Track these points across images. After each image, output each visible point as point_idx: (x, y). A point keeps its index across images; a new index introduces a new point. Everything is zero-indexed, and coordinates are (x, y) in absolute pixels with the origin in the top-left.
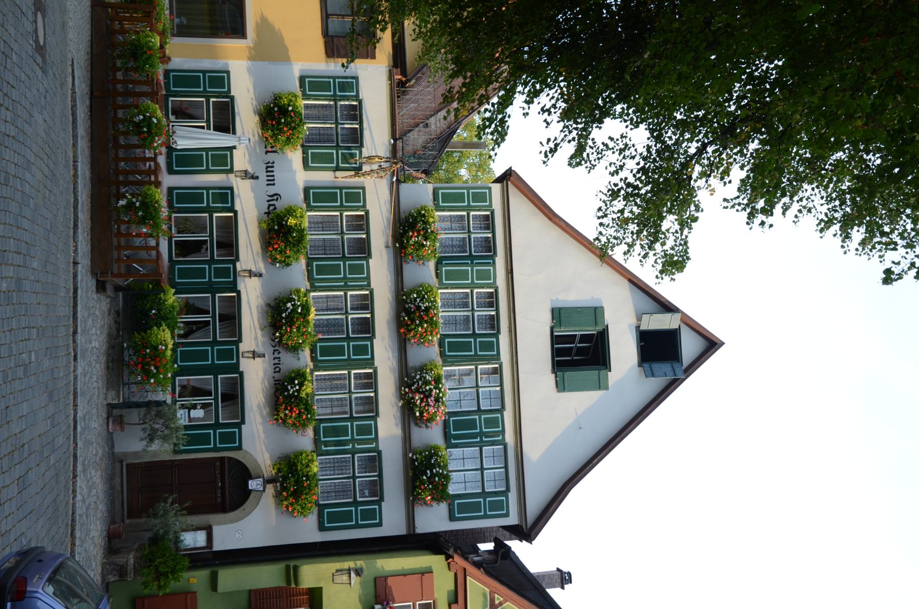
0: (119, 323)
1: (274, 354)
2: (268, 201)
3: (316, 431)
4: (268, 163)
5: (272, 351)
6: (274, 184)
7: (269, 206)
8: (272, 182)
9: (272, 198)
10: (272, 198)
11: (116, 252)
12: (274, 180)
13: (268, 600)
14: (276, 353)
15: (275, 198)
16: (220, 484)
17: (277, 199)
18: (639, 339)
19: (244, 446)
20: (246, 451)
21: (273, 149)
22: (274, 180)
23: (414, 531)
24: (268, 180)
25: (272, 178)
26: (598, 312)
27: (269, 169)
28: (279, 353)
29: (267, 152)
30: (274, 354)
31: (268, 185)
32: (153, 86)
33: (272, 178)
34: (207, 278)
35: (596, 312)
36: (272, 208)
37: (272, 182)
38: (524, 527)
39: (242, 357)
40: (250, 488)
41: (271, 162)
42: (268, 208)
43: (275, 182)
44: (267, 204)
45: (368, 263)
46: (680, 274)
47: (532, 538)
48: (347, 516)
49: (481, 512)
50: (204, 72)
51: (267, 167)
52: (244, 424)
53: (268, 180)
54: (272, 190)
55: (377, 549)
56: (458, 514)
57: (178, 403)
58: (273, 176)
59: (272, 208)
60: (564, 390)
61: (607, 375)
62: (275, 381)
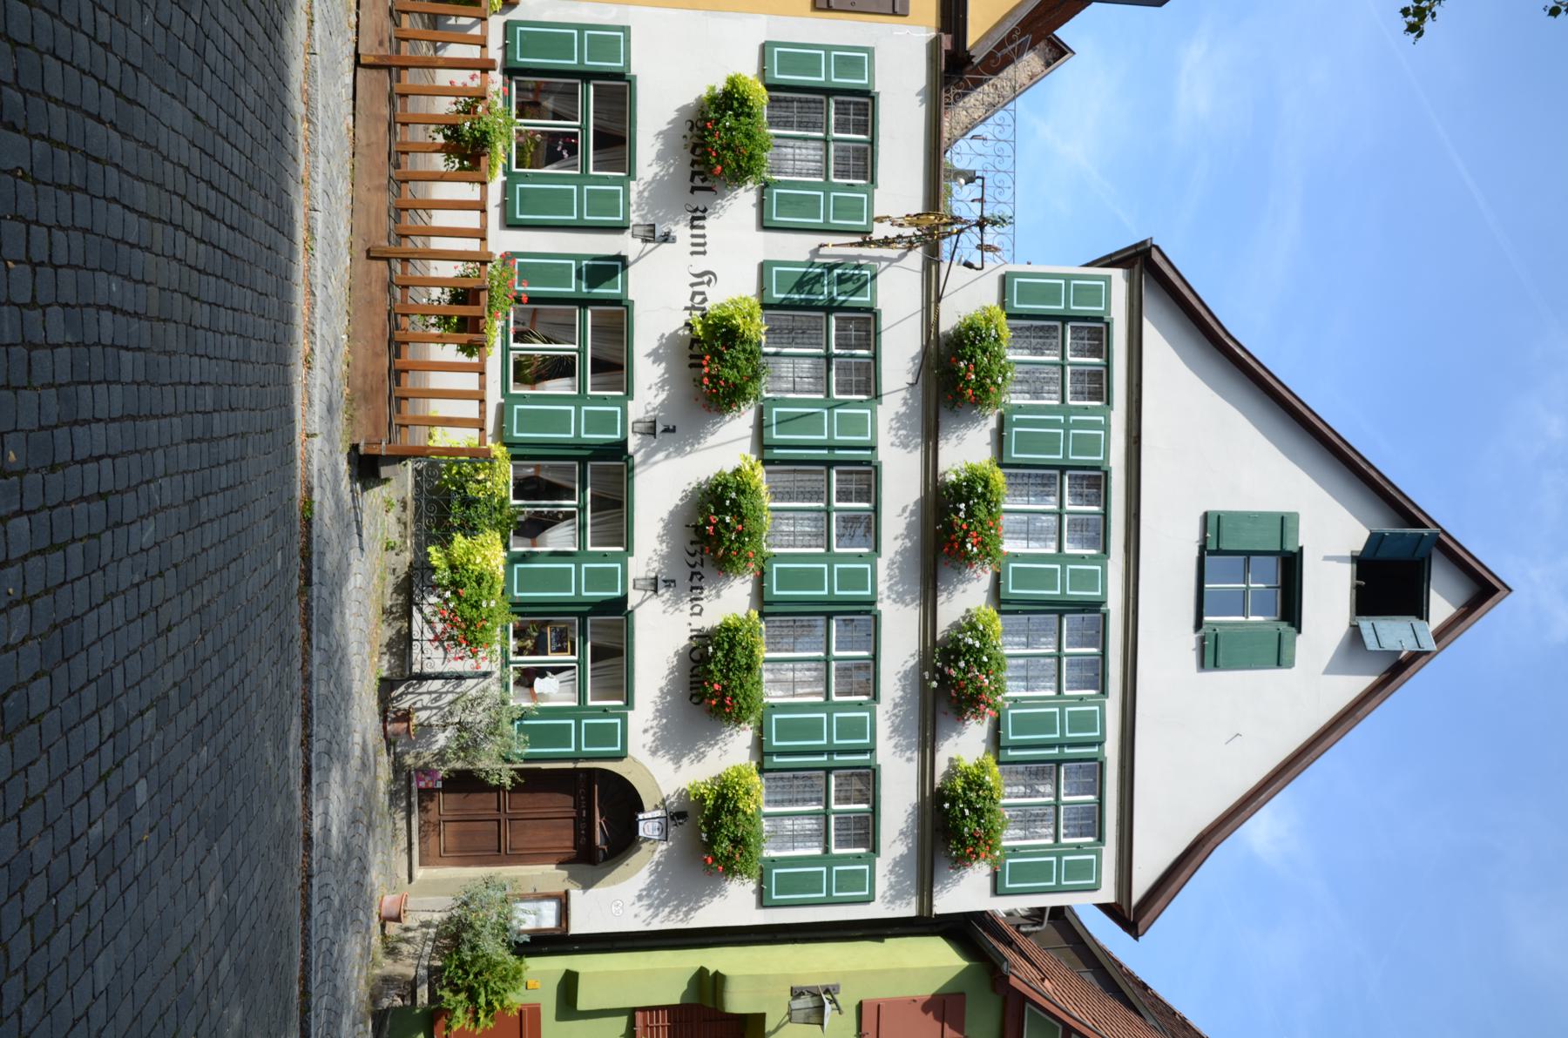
0: (405, 524)
1: (691, 579)
2: (692, 285)
3: (761, 729)
4: (696, 210)
5: (690, 574)
6: (704, 253)
7: (694, 294)
8: (701, 249)
9: (700, 280)
10: (700, 280)
11: (491, 56)
12: (704, 245)
13: (661, 1023)
14: (695, 578)
15: (706, 279)
16: (584, 812)
17: (709, 282)
18: (1355, 575)
19: (630, 751)
20: (634, 760)
21: (706, 184)
22: (704, 245)
23: (931, 911)
24: (693, 245)
25: (701, 241)
26: (1288, 524)
27: (696, 223)
28: (700, 580)
29: (693, 190)
30: (691, 579)
31: (693, 253)
32: (395, 753)
33: (701, 241)
34: (589, 467)
35: (1284, 523)
36: (698, 299)
37: (701, 249)
38: (1125, 907)
39: (634, 588)
40: (641, 833)
41: (701, 208)
42: (692, 299)
43: (707, 248)
44: (690, 290)
45: (874, 413)
46: (987, 304)
47: (1140, 931)
48: (812, 883)
49: (823, 589)
50: (581, 28)
51: (694, 219)
52: (632, 708)
53: (693, 245)
54: (701, 264)
55: (860, 934)
56: (1010, 883)
57: (511, 666)
58: (703, 236)
59: (698, 299)
60: (1216, 666)
61: (1294, 641)
62: (692, 630)
